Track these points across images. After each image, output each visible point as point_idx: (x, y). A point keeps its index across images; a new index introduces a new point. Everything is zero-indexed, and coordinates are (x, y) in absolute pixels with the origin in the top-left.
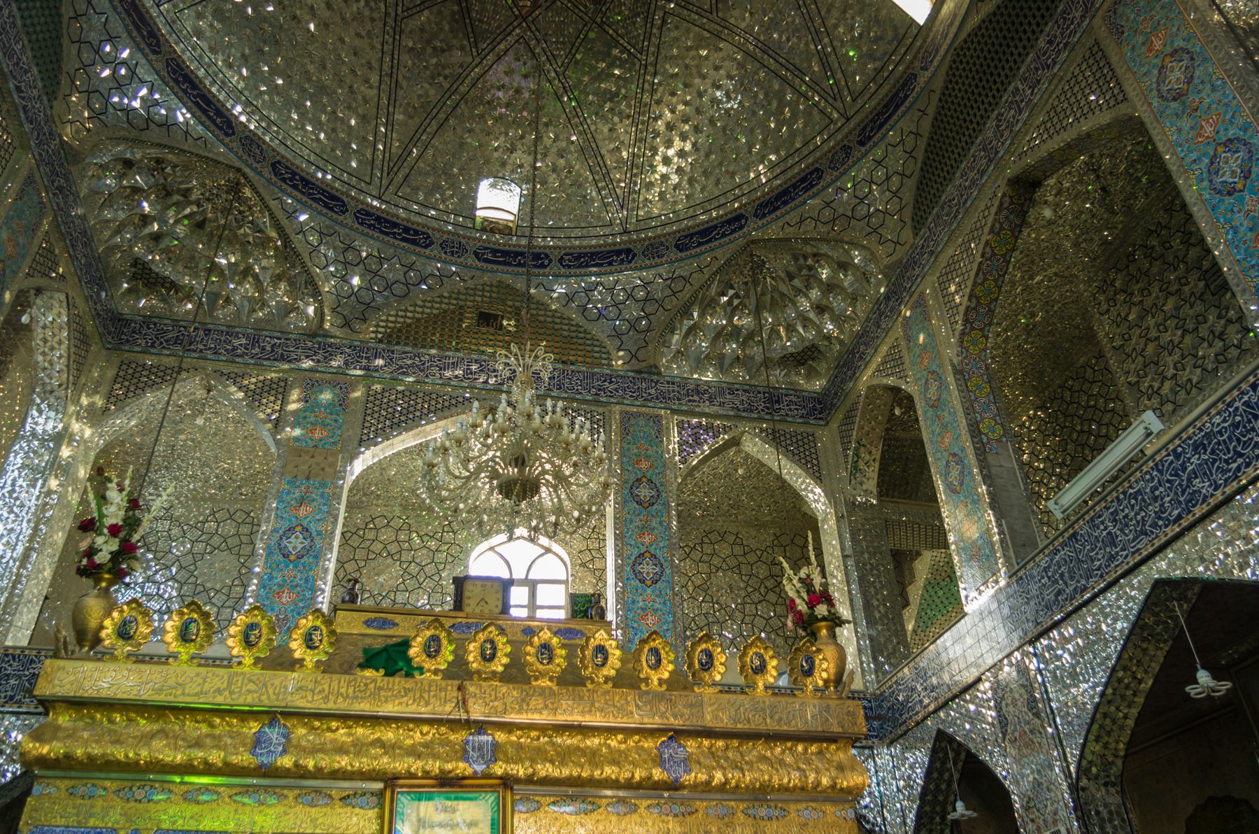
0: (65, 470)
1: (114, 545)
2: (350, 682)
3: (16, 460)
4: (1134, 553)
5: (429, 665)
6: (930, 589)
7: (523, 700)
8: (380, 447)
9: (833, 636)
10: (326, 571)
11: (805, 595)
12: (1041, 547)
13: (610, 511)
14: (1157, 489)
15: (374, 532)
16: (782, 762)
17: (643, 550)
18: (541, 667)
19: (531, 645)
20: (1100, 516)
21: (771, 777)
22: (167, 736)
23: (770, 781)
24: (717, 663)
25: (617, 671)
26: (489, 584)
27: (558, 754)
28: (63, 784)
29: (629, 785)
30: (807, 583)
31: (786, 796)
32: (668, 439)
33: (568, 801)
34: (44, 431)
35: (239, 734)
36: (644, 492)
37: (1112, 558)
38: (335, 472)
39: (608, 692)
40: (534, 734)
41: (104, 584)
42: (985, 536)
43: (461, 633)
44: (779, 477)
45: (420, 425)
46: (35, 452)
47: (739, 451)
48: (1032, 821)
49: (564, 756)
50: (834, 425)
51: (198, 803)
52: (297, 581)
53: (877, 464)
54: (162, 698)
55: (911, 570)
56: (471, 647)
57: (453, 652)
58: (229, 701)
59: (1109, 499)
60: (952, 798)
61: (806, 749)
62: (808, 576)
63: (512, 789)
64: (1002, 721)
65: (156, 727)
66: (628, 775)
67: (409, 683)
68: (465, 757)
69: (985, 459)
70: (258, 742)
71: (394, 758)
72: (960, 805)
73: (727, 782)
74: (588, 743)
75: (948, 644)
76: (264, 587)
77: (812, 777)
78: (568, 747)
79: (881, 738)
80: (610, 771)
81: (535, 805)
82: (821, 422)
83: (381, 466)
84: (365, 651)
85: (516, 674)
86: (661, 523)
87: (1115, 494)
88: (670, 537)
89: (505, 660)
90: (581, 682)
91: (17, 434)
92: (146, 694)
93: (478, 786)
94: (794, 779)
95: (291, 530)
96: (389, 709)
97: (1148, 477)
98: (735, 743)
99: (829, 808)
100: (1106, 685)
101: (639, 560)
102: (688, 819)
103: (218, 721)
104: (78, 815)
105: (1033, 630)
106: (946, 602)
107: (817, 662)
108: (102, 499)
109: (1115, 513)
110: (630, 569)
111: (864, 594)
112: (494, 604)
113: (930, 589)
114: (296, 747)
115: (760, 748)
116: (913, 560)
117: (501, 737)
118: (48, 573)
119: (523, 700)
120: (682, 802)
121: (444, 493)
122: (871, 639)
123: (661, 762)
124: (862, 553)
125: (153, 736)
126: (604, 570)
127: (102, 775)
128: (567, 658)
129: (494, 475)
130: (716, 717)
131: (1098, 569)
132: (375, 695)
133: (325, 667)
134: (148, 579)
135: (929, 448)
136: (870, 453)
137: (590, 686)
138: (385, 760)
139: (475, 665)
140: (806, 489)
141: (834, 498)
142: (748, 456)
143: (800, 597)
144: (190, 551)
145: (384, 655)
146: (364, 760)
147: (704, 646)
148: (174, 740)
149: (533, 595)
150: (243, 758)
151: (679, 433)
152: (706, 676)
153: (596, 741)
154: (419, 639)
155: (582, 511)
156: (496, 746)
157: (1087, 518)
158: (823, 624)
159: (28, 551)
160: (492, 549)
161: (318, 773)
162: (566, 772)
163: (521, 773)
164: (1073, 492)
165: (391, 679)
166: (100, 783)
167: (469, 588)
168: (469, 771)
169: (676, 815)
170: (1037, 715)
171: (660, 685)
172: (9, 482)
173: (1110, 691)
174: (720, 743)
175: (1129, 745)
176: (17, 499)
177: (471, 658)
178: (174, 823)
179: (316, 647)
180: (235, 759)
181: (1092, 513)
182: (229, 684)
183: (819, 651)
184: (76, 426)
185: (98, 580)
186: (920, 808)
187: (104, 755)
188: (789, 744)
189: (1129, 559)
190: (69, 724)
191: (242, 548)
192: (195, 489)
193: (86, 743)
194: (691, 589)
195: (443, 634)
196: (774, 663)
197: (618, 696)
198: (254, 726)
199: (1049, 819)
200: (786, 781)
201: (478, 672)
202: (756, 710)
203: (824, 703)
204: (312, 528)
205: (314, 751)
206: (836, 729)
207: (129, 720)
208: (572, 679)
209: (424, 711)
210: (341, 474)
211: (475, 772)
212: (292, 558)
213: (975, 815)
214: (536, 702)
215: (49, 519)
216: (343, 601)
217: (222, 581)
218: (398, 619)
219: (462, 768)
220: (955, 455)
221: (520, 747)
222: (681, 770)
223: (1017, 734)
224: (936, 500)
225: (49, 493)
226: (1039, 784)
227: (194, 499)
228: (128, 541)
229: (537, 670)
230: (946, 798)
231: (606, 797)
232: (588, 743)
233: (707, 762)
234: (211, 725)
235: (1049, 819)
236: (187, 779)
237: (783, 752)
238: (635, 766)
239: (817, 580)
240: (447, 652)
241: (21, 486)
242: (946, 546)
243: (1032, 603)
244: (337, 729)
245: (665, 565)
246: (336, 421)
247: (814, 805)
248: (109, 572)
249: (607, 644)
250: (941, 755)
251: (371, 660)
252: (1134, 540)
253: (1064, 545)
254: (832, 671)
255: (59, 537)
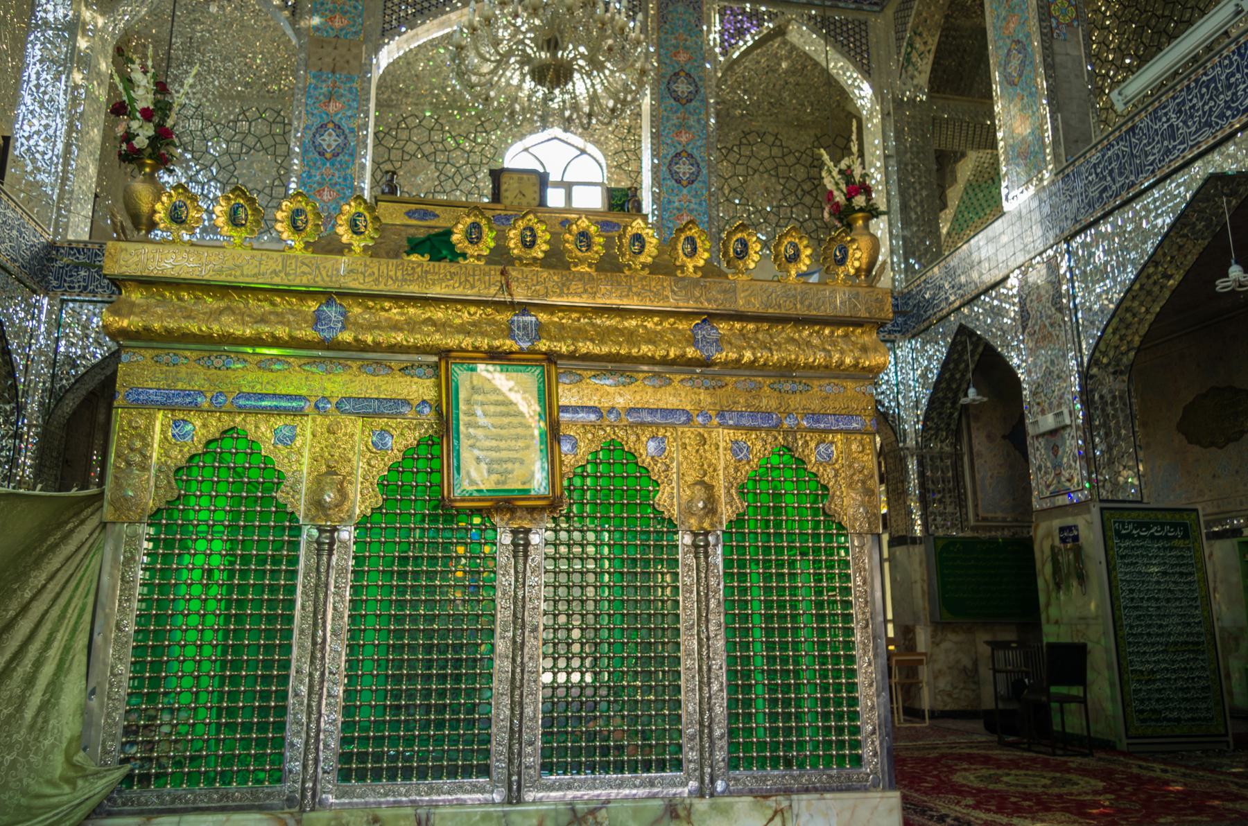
0: (85, 62)
1: (149, 130)
2: (397, 266)
3: (35, 52)
4: (1192, 147)
5: (471, 250)
6: (970, 191)
7: (564, 285)
8: (404, 37)
9: (866, 227)
10: (363, 167)
11: (843, 187)
12: (1094, 142)
13: (646, 102)
14: (1233, 75)
15: (406, 132)
16: (808, 344)
17: (680, 149)
18: (579, 254)
19: (570, 232)
20: (1165, 107)
21: (797, 356)
22: (234, 313)
23: (796, 360)
24: (751, 252)
25: (654, 258)
26: (525, 176)
27: (598, 334)
28: (149, 354)
29: (664, 361)
30: (847, 174)
31: (811, 373)
32: (709, 27)
33: (608, 374)
34: (56, 19)
35: (300, 312)
36: (682, 88)
37: (1168, 152)
38: (361, 65)
39: (645, 278)
40: (574, 315)
41: (147, 170)
42: (1037, 132)
43: (502, 222)
44: (825, 71)
45: (444, 13)
46: (50, 42)
47: (785, 43)
48: (1038, 404)
49: (603, 335)
50: (890, 12)
51: (272, 371)
52: (336, 179)
53: (931, 56)
54: (223, 278)
55: (953, 172)
56: (512, 233)
57: (494, 239)
58: (286, 282)
59: (1178, 88)
60: (964, 386)
61: (832, 333)
62: (849, 167)
63: (555, 363)
64: (1024, 314)
65: (222, 304)
66: (663, 353)
67: (454, 268)
68: (511, 335)
69: (1051, 46)
70: (318, 319)
71: (445, 335)
72: (972, 392)
73: (756, 360)
74: (626, 324)
75: (981, 244)
76: (305, 185)
77: (836, 357)
78: (607, 328)
79: (903, 333)
80: (646, 349)
81: (578, 378)
82: (876, 8)
83: (407, 60)
84: (409, 240)
85: (556, 260)
86: (698, 121)
87: (1186, 82)
88: (708, 137)
89: (545, 247)
90: (619, 268)
91: (28, 25)
92: (207, 274)
93: (524, 360)
94: (820, 358)
95: (323, 126)
96: (436, 291)
97: (1227, 62)
98: (766, 326)
99: (850, 384)
100: (1133, 282)
101: (676, 160)
102: (718, 392)
103: (278, 300)
104: (166, 379)
105: (1069, 226)
106: (985, 205)
107: (851, 251)
108: (129, 82)
109: (1183, 103)
110: (665, 173)
111: (902, 193)
112: (532, 195)
113: (970, 191)
114: (354, 324)
115: (789, 330)
116: (956, 162)
117: (543, 317)
118: (92, 170)
119: (564, 285)
120: (714, 376)
121: (474, 79)
122: (904, 239)
123: (694, 342)
124: (906, 153)
125: (221, 312)
126: (639, 173)
127: (182, 346)
128: (604, 246)
129: (525, 60)
130: (749, 302)
131: (1151, 164)
132: (423, 278)
133: (373, 252)
134: (191, 179)
135: (990, 35)
136: (925, 43)
137: (627, 273)
138: (437, 336)
139: (516, 251)
140: (852, 85)
141: (882, 93)
142: (794, 48)
143: (839, 189)
144: (227, 152)
145: (428, 243)
146: (418, 336)
147: (739, 235)
148: (241, 317)
149: (569, 197)
150: (306, 333)
151: (721, 21)
152: (741, 263)
153: (634, 323)
154: (460, 226)
155: (617, 100)
156: (539, 325)
157: (1150, 109)
158: (860, 215)
159: (68, 146)
160: (526, 150)
161: (377, 347)
162: (605, 350)
163: (564, 349)
164: (1139, 83)
165: (437, 264)
166: (181, 352)
167: (508, 185)
168: (515, 348)
169: (707, 388)
170: (1060, 310)
171: (695, 272)
172: (33, 77)
173: (1137, 286)
174: (751, 326)
175: (1145, 339)
176: (45, 93)
177: (512, 245)
178: (253, 387)
179: (362, 233)
180: (299, 334)
181: (1157, 104)
182: (284, 266)
183: (853, 241)
184: (87, 15)
185: (142, 166)
186: (932, 394)
187: (179, 328)
188: (817, 328)
189: (1186, 153)
190: (142, 301)
191: (277, 146)
192: (220, 86)
193: (161, 318)
194: (726, 192)
195: (484, 222)
196: (808, 251)
197: (655, 282)
198: (313, 306)
199: (1055, 403)
200: (811, 360)
201: (520, 258)
202: (787, 296)
203: (854, 290)
204: (344, 124)
205: (371, 327)
206: (863, 314)
207: (197, 298)
208: (610, 266)
209: (470, 294)
210: (367, 68)
211: (521, 349)
212: (328, 156)
213: (985, 399)
214: (576, 286)
215: (82, 114)
216: (383, 193)
217: (264, 182)
218: (438, 210)
219: (508, 344)
220: (1018, 42)
221: (562, 327)
222: (713, 349)
223: (1037, 328)
224: (991, 97)
225: (76, 87)
226: (1051, 373)
227: (221, 96)
228: (163, 126)
229: (576, 257)
230: (959, 386)
231: (643, 372)
232: (626, 324)
233: (738, 343)
234: (273, 304)
235: (1055, 403)
236: (258, 350)
237: (811, 334)
238: (670, 346)
239: (857, 172)
240: (489, 240)
241: (46, 80)
242: (993, 145)
243: (1075, 201)
244: (390, 309)
245: (702, 164)
246: (355, 8)
247: (836, 381)
248: (150, 157)
249: (644, 233)
250: (959, 348)
251: (415, 246)
252: (1196, 132)
253: (1120, 138)
254: (865, 260)
255: (96, 134)
